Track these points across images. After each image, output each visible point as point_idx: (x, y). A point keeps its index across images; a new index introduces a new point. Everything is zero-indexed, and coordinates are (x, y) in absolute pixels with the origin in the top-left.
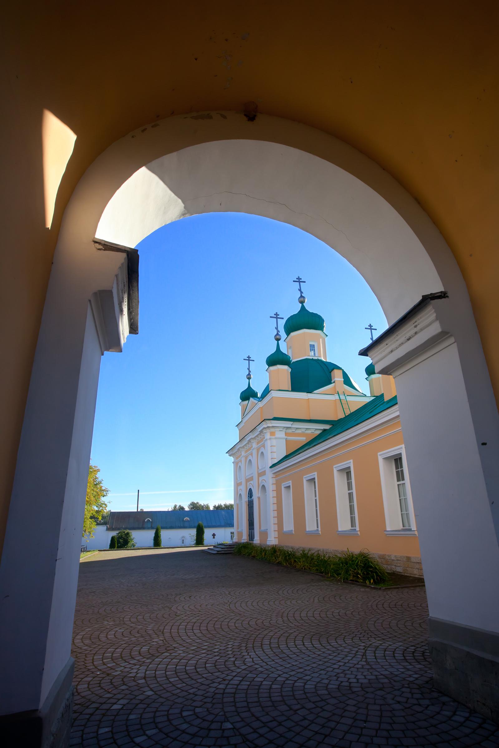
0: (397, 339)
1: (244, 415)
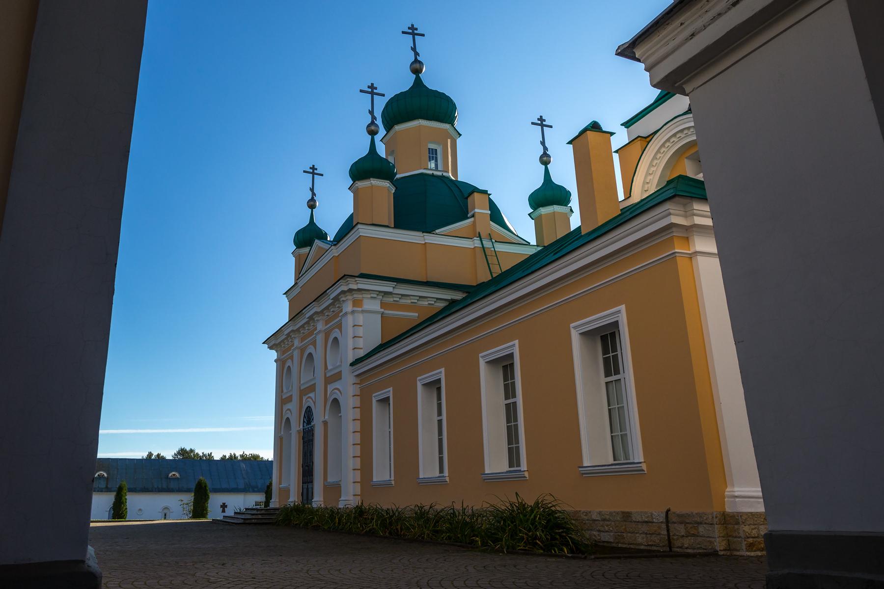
0: (706, 8)
1: (297, 279)
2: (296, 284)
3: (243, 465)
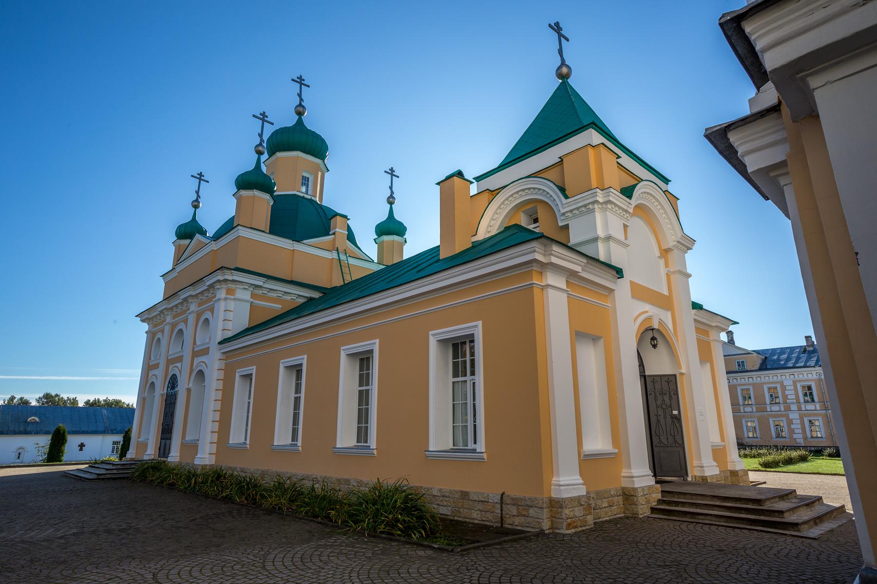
1: (178, 260)
2: (173, 269)
3: (105, 412)
